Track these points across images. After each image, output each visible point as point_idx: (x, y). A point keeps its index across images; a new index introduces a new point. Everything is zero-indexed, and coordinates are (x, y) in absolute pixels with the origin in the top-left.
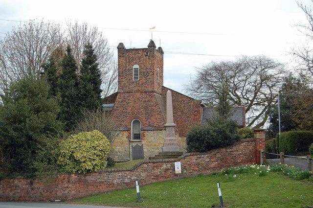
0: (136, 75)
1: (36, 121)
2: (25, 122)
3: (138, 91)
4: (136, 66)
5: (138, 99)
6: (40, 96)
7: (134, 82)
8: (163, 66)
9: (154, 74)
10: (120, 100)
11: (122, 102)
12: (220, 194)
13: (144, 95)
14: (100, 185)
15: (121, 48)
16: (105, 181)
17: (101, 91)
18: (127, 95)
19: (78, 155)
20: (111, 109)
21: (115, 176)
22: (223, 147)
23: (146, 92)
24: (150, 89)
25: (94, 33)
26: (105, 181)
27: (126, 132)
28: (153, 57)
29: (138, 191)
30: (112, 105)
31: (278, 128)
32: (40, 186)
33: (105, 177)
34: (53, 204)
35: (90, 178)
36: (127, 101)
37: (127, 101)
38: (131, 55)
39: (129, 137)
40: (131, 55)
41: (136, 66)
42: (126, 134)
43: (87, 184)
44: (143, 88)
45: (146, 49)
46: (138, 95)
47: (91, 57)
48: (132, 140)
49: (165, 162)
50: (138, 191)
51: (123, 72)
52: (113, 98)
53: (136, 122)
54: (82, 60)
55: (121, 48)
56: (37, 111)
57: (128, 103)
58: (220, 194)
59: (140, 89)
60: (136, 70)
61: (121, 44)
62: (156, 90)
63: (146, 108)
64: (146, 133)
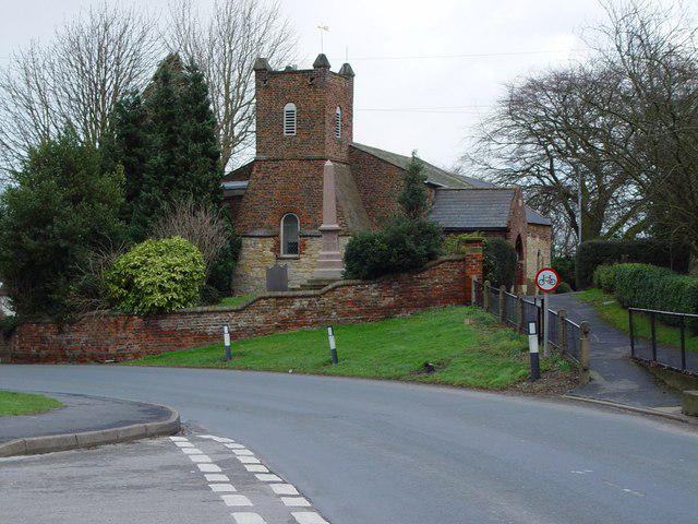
0: (290, 122)
1: (75, 220)
2: (52, 224)
6: (83, 172)
7: (285, 140)
8: (352, 103)
9: (324, 123)
12: (333, 346)
19: (142, 280)
20: (242, 192)
22: (403, 272)
24: (316, 155)
25: (272, 16)
29: (227, 343)
30: (245, 183)
32: (80, 338)
34: (81, 366)
35: (165, 324)
38: (281, 83)
39: (276, 249)
40: (281, 83)
41: (291, 107)
42: (270, 243)
43: (159, 333)
45: (311, 71)
46: (295, 164)
47: (197, 89)
48: (282, 255)
49: (298, 297)
50: (227, 343)
51: (267, 120)
52: (243, 173)
53: (290, 220)
54: (24, 154)
55: (262, 71)
56: (76, 200)
58: (333, 346)
64: (309, 242)
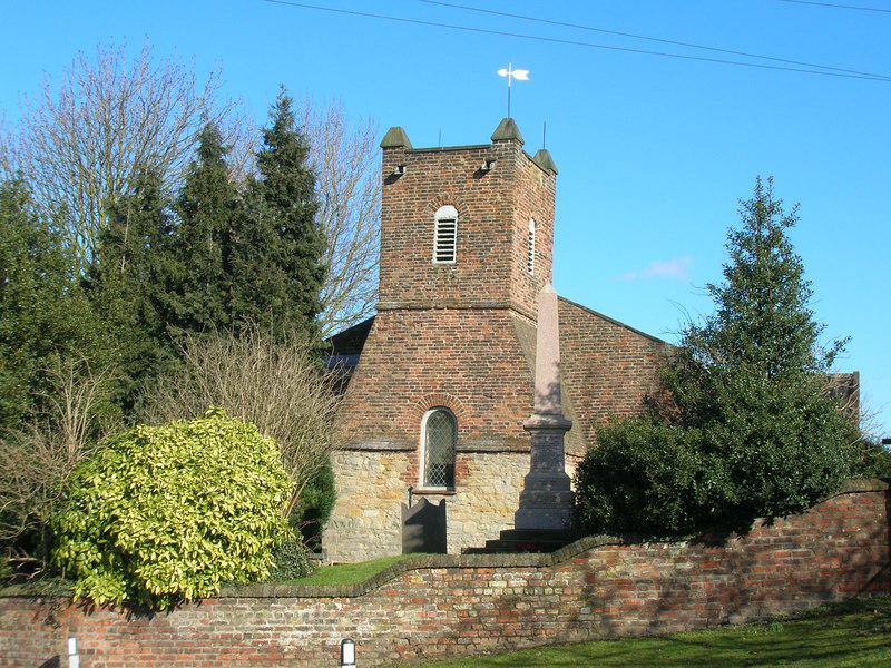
0: (446, 243)
3: (452, 306)
4: (447, 212)
5: (450, 332)
10: (384, 337)
11: (390, 342)
13: (473, 319)
14: (225, 652)
15: (394, 147)
16: (247, 636)
17: (686, 428)
18: (409, 317)
21: (288, 616)
23: (477, 308)
26: (247, 636)
27: (403, 455)
28: (509, 177)
31: (445, 265)
33: (245, 619)
36: (409, 340)
37: (409, 340)
38: (433, 170)
41: (447, 212)
44: (472, 294)
45: (487, 147)
46: (450, 318)
55: (394, 147)
57: (412, 349)
59: (457, 296)
60: (446, 224)
61: (396, 132)
62: (520, 301)
63: (477, 368)
